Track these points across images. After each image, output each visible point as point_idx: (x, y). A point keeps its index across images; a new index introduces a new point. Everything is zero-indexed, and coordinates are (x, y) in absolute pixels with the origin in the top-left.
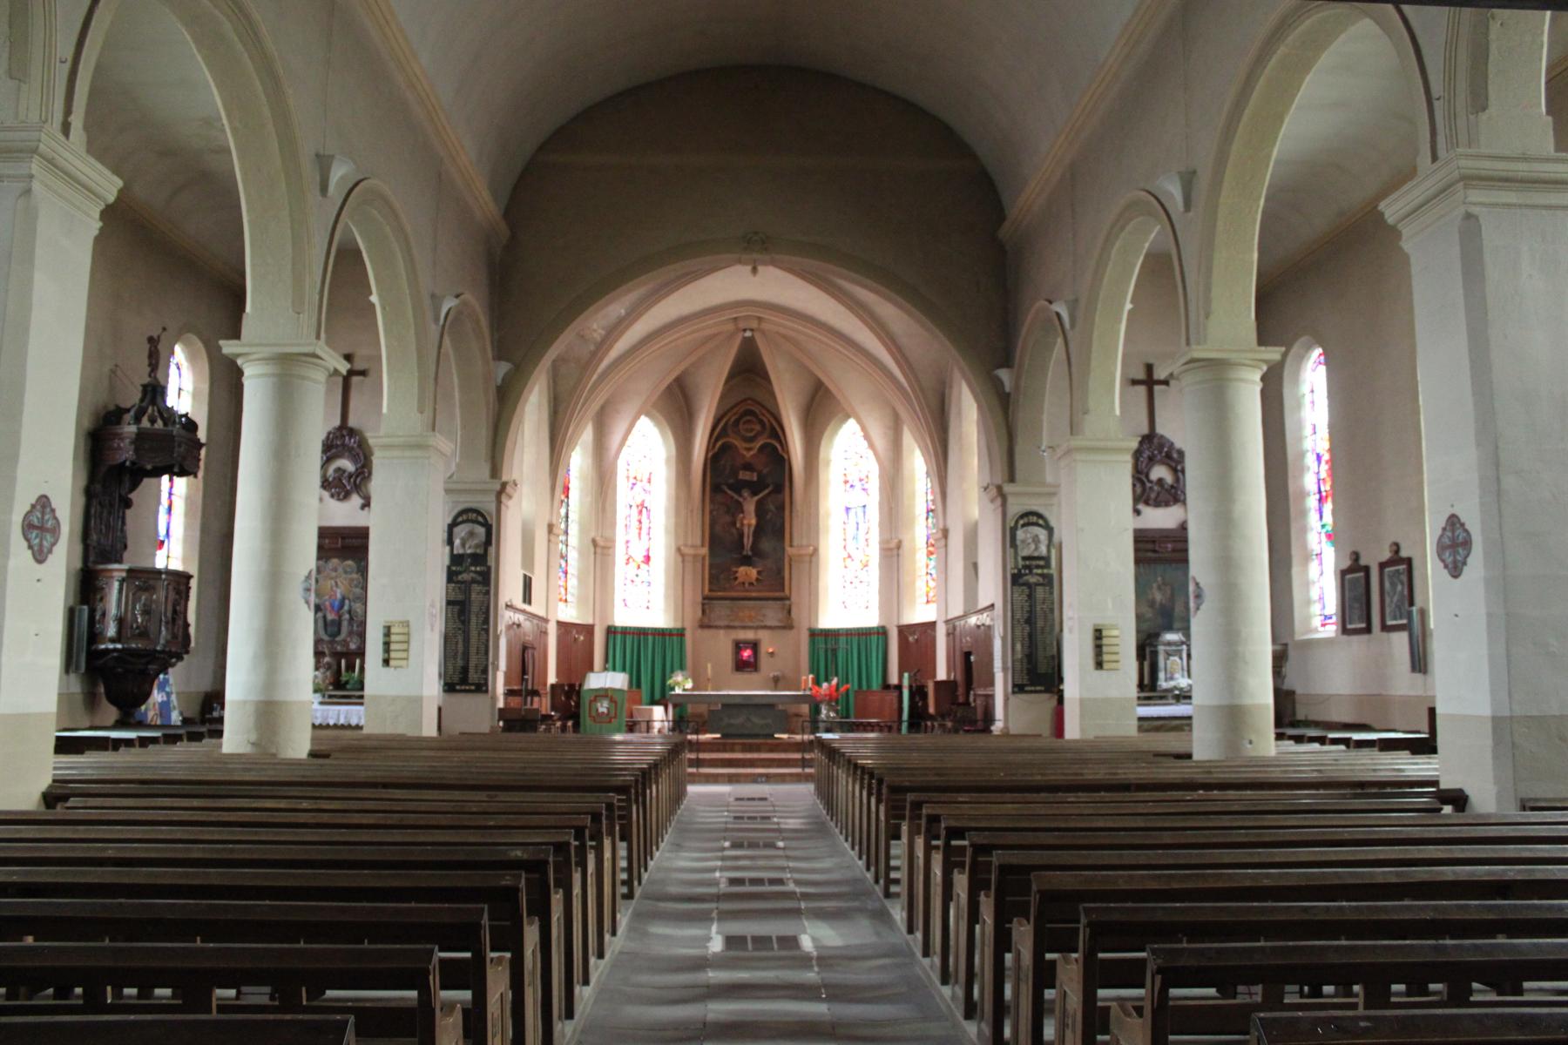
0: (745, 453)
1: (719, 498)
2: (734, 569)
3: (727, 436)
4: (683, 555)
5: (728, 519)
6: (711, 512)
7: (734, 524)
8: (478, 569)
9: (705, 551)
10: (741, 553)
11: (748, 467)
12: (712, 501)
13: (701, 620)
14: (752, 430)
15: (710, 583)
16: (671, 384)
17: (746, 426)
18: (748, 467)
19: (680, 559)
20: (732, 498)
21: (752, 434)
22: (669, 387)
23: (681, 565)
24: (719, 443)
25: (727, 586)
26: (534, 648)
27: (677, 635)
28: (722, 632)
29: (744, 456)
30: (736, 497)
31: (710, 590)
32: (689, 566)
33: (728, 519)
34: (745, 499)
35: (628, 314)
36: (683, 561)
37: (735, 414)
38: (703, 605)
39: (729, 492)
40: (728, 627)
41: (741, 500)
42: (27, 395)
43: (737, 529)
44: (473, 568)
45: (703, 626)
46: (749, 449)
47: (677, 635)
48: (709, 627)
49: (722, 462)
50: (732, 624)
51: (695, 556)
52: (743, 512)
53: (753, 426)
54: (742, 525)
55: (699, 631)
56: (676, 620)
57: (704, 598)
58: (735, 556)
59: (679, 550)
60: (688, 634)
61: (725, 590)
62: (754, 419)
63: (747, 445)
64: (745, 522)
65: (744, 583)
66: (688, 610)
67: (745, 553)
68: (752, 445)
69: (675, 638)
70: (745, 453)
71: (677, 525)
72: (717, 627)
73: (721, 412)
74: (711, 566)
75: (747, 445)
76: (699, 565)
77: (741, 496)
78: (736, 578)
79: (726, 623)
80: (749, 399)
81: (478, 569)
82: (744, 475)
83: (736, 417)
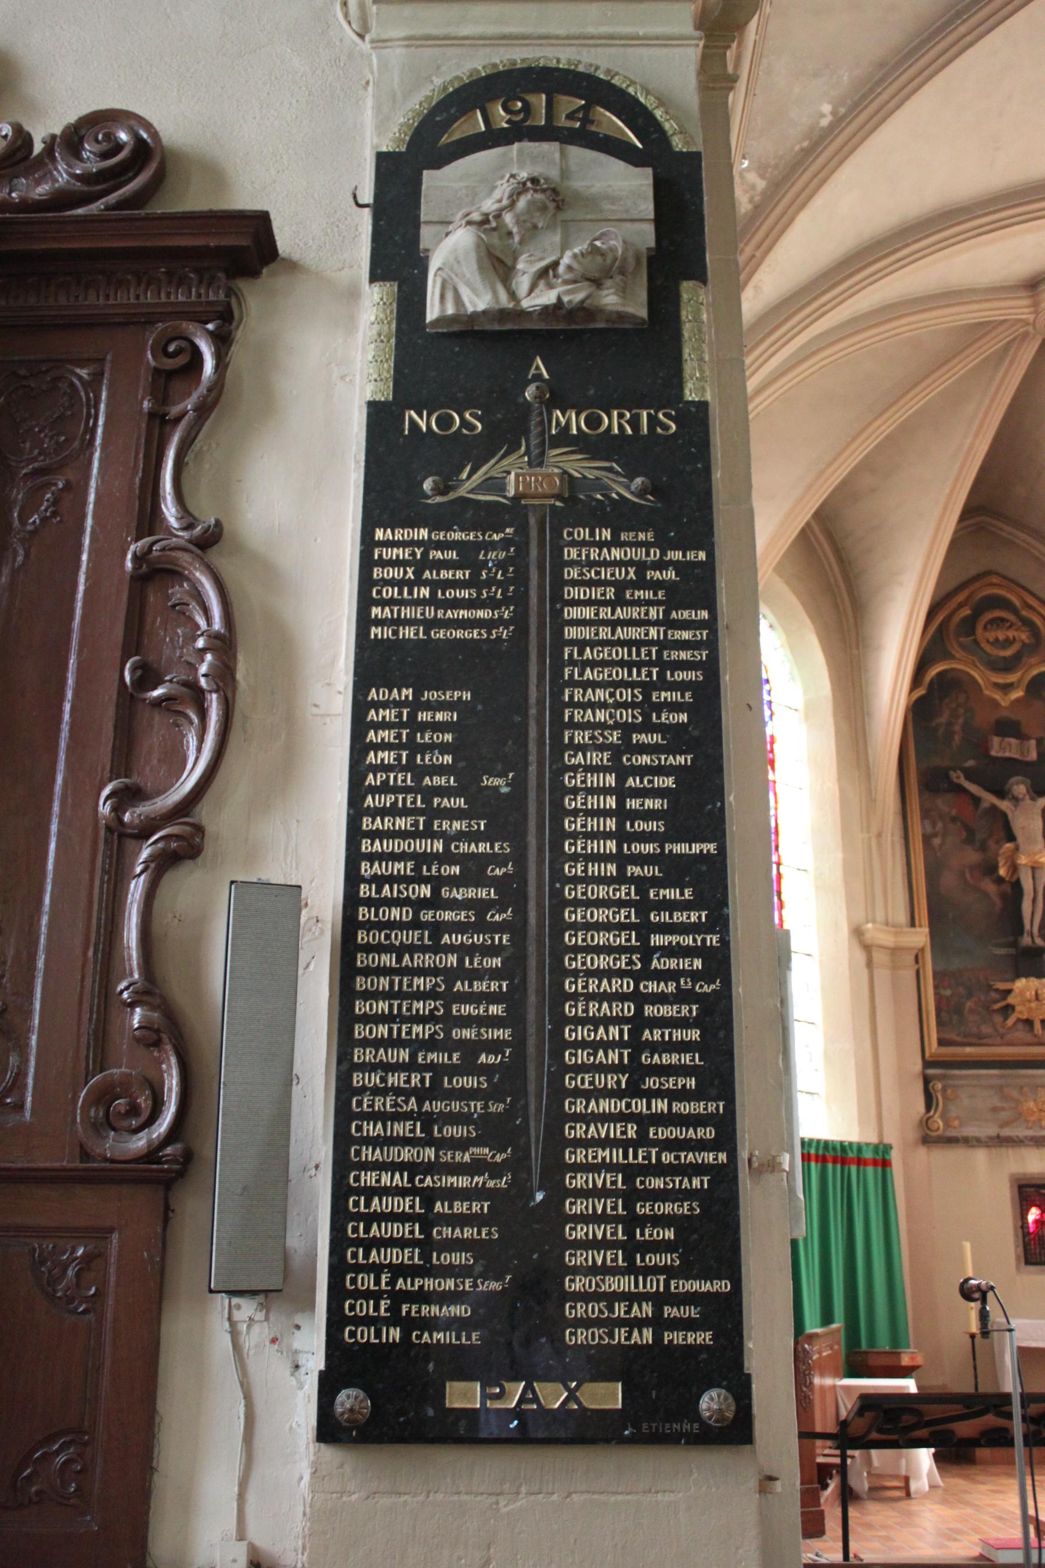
0: (997, 696)
1: (943, 803)
2: (1002, 986)
3: (948, 656)
4: (867, 948)
5: (972, 856)
6: (927, 839)
7: (991, 869)
8: (613, 422)
9: (920, 937)
10: (1014, 944)
11: (1008, 728)
12: (925, 814)
13: (925, 1123)
14: (1008, 642)
15: (940, 1023)
16: (808, 524)
17: (991, 635)
18: (1008, 728)
19: (861, 957)
20: (976, 800)
21: (1008, 653)
22: (804, 535)
23: (865, 972)
24: (933, 672)
25: (986, 1029)
26: (992, 1288)
27: (875, 1163)
28: (980, 1156)
29: (995, 704)
30: (989, 799)
31: (941, 1042)
32: (883, 975)
33: (972, 856)
34: (1016, 800)
35: (839, 122)
36: (869, 964)
37: (961, 606)
38: (927, 1080)
39: (973, 788)
40: (1001, 1142)
41: (1004, 805)
42: (826, 1521)
43: (1000, 880)
44: (576, 422)
45: (929, 1138)
46: (1006, 688)
47: (875, 1163)
48: (951, 1141)
49: (943, 719)
50: (1006, 1132)
51: (895, 951)
52: (1011, 837)
53: (1011, 634)
54: (1014, 868)
55: (922, 1151)
56: (862, 1122)
57: (927, 1064)
58: (1002, 951)
59: (857, 932)
60: (895, 1156)
61: (979, 1040)
62: (1012, 617)
63: (1000, 679)
64: (1023, 860)
65: (1029, 1023)
66: (890, 1097)
67: (1026, 940)
68: (1012, 678)
69: (870, 1169)
70: (997, 696)
71: (848, 868)
72: (967, 1142)
73: (952, 585)
74: (939, 977)
75: (1000, 679)
76: (908, 975)
77: (1001, 794)
78: (1009, 1009)
79: (992, 1130)
80: (989, 573)
81: (613, 422)
82: (1002, 748)
83: (966, 612)
